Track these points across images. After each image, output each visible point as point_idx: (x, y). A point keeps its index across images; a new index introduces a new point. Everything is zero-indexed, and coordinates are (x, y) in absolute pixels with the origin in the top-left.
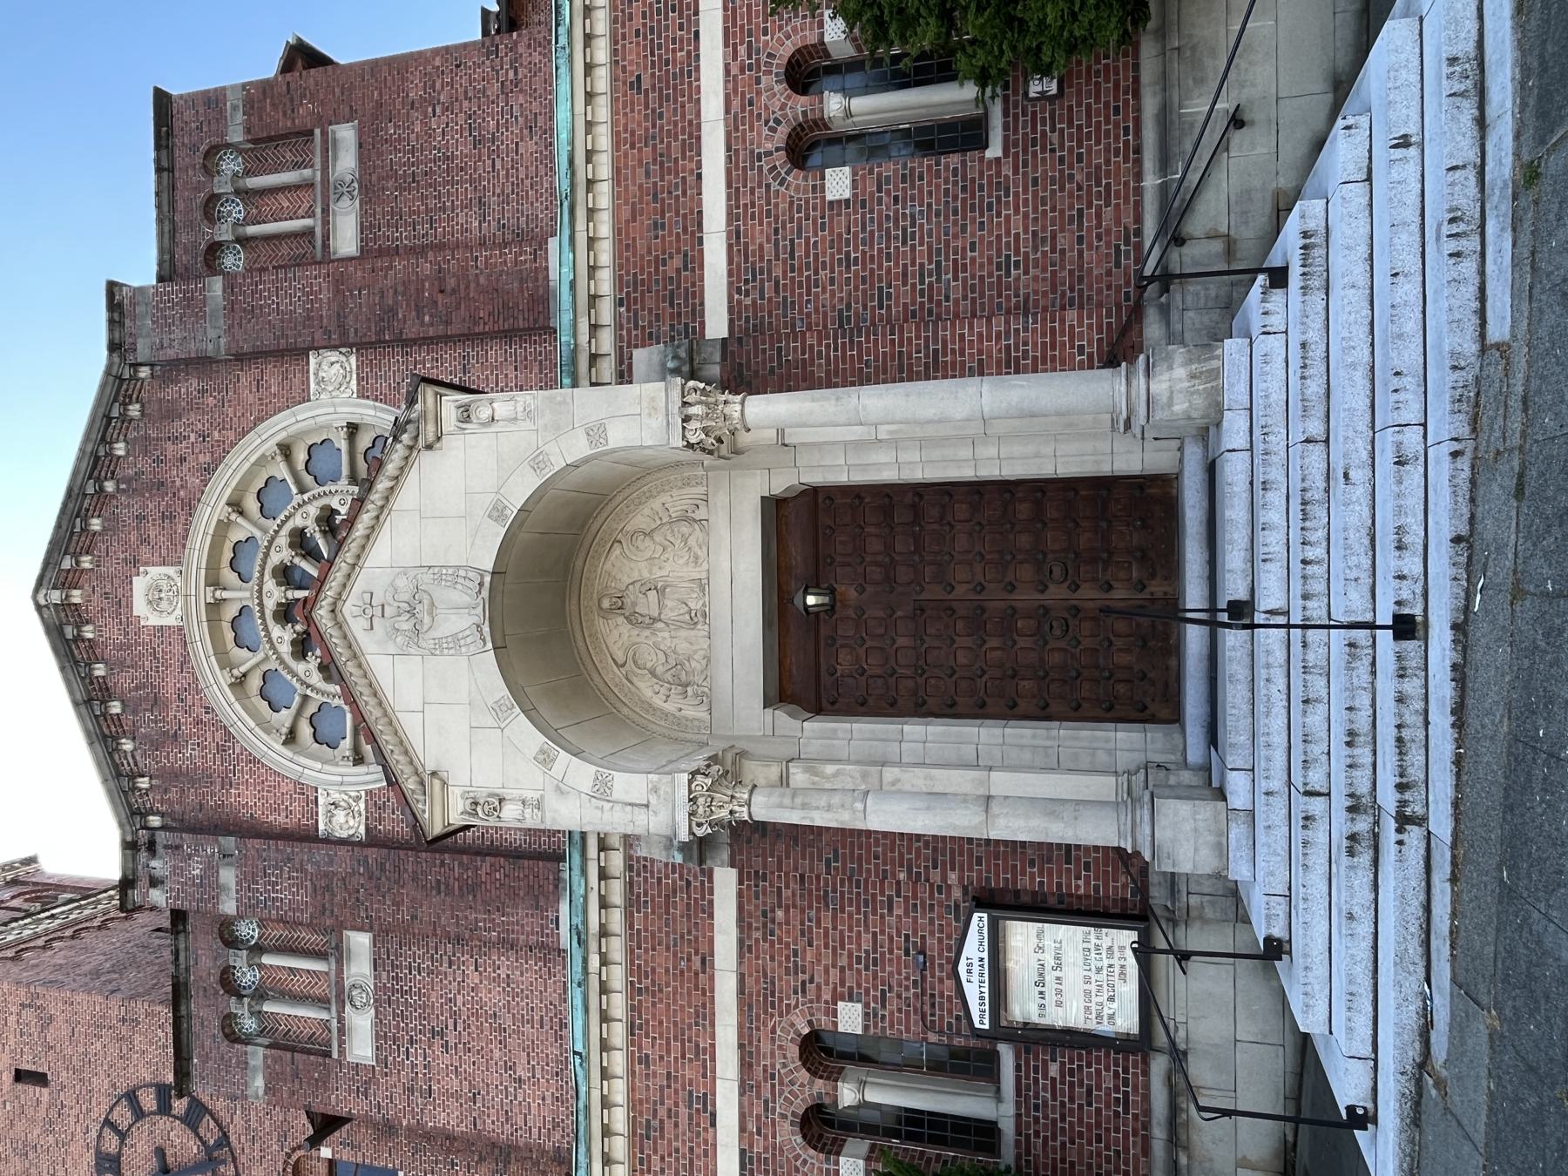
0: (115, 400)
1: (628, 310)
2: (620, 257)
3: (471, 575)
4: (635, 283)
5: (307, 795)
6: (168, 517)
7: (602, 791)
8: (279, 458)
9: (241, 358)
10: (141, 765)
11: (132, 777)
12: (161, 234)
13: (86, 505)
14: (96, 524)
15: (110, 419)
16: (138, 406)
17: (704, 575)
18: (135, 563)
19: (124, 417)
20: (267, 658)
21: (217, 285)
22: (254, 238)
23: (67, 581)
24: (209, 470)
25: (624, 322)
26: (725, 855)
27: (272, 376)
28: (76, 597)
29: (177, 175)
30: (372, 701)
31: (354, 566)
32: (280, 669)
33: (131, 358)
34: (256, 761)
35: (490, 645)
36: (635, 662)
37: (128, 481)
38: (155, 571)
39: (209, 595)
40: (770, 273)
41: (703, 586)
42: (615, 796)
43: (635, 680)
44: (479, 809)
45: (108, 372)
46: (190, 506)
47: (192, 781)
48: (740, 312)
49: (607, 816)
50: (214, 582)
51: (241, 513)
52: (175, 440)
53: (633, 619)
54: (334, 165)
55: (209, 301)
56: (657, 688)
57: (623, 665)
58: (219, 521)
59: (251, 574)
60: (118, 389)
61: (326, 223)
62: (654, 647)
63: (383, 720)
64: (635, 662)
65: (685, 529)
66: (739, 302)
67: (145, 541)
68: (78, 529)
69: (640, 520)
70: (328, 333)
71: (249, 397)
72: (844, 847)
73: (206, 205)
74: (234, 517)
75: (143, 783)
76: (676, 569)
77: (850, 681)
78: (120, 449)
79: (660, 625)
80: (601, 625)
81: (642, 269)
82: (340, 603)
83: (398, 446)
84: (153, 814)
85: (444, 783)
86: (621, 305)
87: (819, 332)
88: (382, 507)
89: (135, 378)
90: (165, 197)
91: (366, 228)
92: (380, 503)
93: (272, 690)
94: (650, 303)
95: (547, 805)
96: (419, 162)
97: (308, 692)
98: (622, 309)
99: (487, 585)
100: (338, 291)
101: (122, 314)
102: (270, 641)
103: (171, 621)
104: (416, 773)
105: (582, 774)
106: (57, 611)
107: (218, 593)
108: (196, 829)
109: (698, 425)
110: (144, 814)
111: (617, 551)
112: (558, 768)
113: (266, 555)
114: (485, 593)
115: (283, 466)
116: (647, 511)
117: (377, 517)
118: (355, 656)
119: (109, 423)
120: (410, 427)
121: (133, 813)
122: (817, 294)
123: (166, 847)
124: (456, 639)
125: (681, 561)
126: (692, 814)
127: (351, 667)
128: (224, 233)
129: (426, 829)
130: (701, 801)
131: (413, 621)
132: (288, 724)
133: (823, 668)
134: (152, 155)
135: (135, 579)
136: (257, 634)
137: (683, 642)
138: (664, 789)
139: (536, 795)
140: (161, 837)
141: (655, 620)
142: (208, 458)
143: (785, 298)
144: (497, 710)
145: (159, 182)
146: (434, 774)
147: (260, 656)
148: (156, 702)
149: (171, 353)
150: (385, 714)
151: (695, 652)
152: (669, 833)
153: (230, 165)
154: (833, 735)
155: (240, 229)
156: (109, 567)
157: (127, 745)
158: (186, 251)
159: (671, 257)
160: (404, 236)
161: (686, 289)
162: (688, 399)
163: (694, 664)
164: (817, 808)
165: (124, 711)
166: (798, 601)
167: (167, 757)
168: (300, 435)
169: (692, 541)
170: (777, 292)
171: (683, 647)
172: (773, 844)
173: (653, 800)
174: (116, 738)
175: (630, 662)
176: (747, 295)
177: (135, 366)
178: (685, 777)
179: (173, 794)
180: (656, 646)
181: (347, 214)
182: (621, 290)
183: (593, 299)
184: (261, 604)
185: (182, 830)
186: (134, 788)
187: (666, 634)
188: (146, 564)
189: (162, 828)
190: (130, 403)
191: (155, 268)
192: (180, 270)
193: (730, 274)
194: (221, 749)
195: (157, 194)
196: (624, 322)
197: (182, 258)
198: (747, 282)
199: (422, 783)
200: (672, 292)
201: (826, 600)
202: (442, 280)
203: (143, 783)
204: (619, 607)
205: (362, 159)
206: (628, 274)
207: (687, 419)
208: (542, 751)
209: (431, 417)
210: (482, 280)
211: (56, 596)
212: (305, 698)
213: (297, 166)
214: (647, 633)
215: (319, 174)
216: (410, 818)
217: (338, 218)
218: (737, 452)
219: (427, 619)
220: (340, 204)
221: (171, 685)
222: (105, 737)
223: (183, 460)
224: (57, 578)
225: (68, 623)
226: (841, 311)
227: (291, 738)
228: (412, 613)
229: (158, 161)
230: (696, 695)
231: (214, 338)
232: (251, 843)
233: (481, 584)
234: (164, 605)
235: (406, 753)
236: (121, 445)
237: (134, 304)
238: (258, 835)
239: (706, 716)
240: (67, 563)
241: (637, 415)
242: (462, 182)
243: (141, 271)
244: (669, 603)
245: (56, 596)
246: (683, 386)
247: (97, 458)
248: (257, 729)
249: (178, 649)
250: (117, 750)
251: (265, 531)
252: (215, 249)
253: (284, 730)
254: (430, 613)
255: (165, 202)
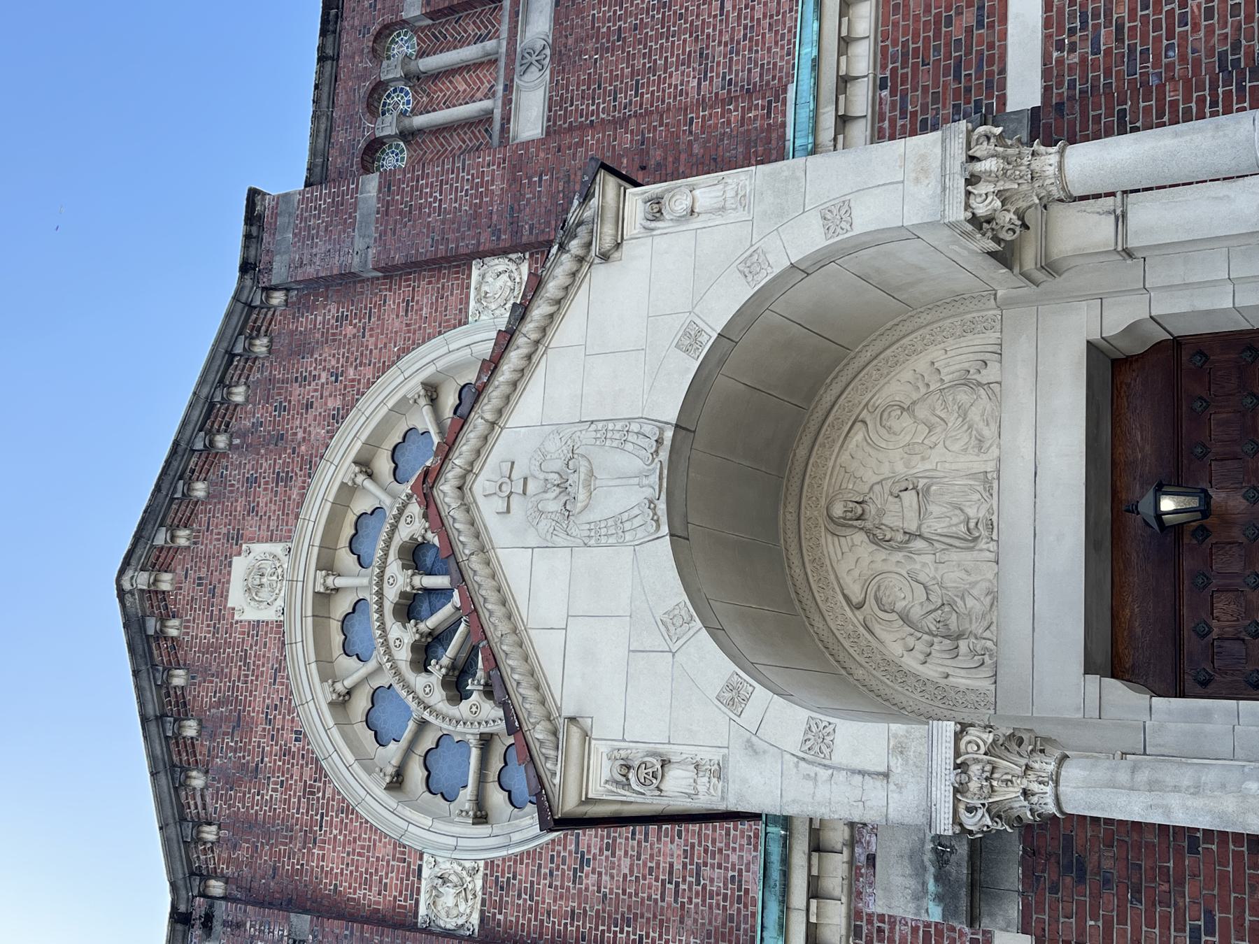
0: (240, 334)
1: (893, 94)
2: (885, 24)
3: (647, 429)
4: (905, 55)
5: (409, 862)
6: (283, 479)
7: (816, 748)
8: (423, 401)
9: (391, 273)
10: (210, 810)
11: (198, 824)
12: (315, 134)
13: (192, 465)
14: (200, 490)
15: (231, 356)
16: (265, 341)
17: (990, 467)
18: (237, 539)
19: (249, 357)
20: (380, 668)
21: (371, 183)
22: (420, 131)
23: (159, 561)
24: (338, 417)
25: (887, 108)
26: (1013, 910)
27: (425, 293)
28: (166, 582)
29: (341, 63)
30: (499, 611)
31: (493, 424)
32: (397, 687)
33: (264, 282)
34: (348, 810)
35: (665, 529)
36: (878, 600)
37: (243, 435)
38: (259, 549)
39: (320, 580)
40: (1108, 13)
41: (989, 482)
42: (839, 757)
43: (877, 629)
44: (631, 775)
45: (236, 298)
46: (310, 466)
47: (268, 835)
48: (1061, 76)
49: (823, 791)
50: (327, 565)
51: (370, 476)
52: (303, 380)
53: (878, 540)
54: (524, 31)
55: (361, 205)
56: (911, 641)
57: (859, 607)
58: (343, 484)
59: (372, 557)
60: (246, 317)
61: (507, 102)
62: (908, 579)
63: (510, 639)
64: (878, 600)
65: (963, 396)
66: (1060, 61)
67: (252, 510)
68: (178, 495)
69: (896, 388)
70: (497, 233)
71: (395, 323)
72: (1225, 908)
73: (371, 95)
74: (360, 479)
75: (210, 833)
76: (950, 460)
77: (1236, 647)
78: (239, 394)
79: (919, 544)
80: (830, 546)
81: (916, 35)
82: (470, 477)
83: (565, 257)
84: (216, 878)
85: (586, 735)
86: (883, 86)
87: (1187, 82)
88: (537, 342)
89: (266, 305)
90: (325, 88)
91: (555, 104)
92: (534, 336)
93: (380, 717)
94: (925, 80)
95: (732, 771)
96: (628, 13)
97: (426, 715)
98: (885, 93)
99: (667, 442)
100: (514, 180)
101: (261, 228)
102: (386, 643)
103: (270, 615)
104: (548, 718)
105: (783, 718)
106: (141, 599)
107: (330, 580)
108: (264, 901)
109: (991, 188)
110: (204, 876)
111: (858, 436)
112: (751, 714)
113: (394, 528)
114: (664, 455)
115: (426, 411)
116: (907, 375)
117: (529, 357)
118: (482, 549)
119: (230, 362)
120: (582, 231)
121: (192, 874)
122: (1184, 36)
123: (225, 924)
124: (619, 521)
125: (956, 447)
126: (959, 790)
127: (475, 563)
128: (387, 126)
129: (555, 802)
130: (975, 769)
131: (563, 498)
132: (395, 762)
133: (1188, 625)
134: (316, 41)
135: (235, 559)
136: (371, 639)
137: (954, 570)
138: (916, 748)
139: (716, 756)
140: (221, 909)
141: (911, 536)
142: (338, 403)
143: (1132, 49)
144: (668, 625)
145: (320, 73)
146: (572, 719)
147: (372, 665)
148: (239, 723)
149: (310, 271)
150: (515, 630)
151: (975, 583)
152: (921, 820)
153: (403, 46)
154: (1207, 716)
155: (406, 122)
156: (210, 544)
157: (198, 780)
158: (342, 152)
159: (959, 13)
160: (602, 109)
161: (980, 53)
162: (977, 151)
163: (970, 602)
164: (1176, 789)
165: (200, 733)
166: (1145, 507)
167: (242, 800)
168: (449, 372)
169: (974, 415)
170: (1120, 39)
171: (953, 577)
172: (1096, 896)
173: (897, 765)
174: (185, 770)
175: (871, 601)
176: (1072, 48)
177: (269, 290)
178: (950, 727)
179: (242, 854)
180: (913, 577)
181: (536, 88)
182: (884, 67)
183: (844, 82)
184: (380, 594)
185: (247, 903)
186: (198, 840)
187: (928, 559)
188: (251, 540)
189: (224, 898)
190: (258, 336)
191: (304, 174)
192: (333, 175)
193: (1047, 24)
194: (309, 791)
195: (316, 87)
196: (887, 108)
197: (337, 160)
198: (1072, 32)
199: (555, 733)
200: (959, 61)
201: (1193, 502)
202: (643, 153)
203: (210, 833)
204: (856, 517)
205: (557, 20)
206: (895, 43)
207: (972, 180)
208: (730, 687)
209: (610, 214)
210: (696, 149)
211: (143, 580)
212: (423, 724)
213: (480, 39)
214: (899, 556)
215: (504, 43)
216: (534, 781)
217: (524, 95)
218: (1050, 267)
219: (582, 496)
220: (527, 77)
221: (260, 698)
222: (173, 766)
223: (309, 406)
224: (147, 557)
225: (152, 614)
226: (1223, 55)
227: (397, 782)
228: (563, 487)
229: (321, 49)
230: (973, 652)
231: (361, 250)
232: (328, 924)
233: (659, 442)
234: (264, 594)
235: (537, 688)
236: (241, 389)
237: (275, 215)
238: (340, 916)
239: (987, 685)
240: (161, 538)
241: (891, 191)
242: (681, 31)
243: (285, 175)
244: (935, 509)
245: (143, 580)
246: (969, 133)
247: (212, 405)
248: (356, 766)
249: (273, 652)
250: (184, 785)
251: (394, 496)
252: (375, 147)
253: (390, 770)
254: (588, 485)
255: (325, 96)
